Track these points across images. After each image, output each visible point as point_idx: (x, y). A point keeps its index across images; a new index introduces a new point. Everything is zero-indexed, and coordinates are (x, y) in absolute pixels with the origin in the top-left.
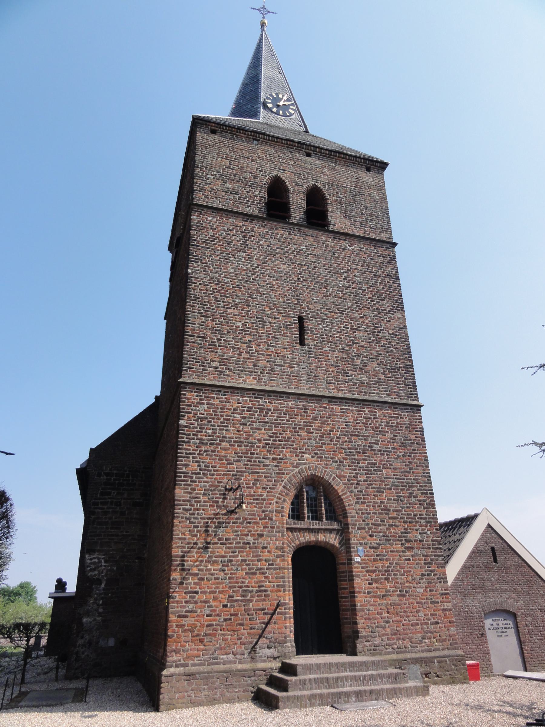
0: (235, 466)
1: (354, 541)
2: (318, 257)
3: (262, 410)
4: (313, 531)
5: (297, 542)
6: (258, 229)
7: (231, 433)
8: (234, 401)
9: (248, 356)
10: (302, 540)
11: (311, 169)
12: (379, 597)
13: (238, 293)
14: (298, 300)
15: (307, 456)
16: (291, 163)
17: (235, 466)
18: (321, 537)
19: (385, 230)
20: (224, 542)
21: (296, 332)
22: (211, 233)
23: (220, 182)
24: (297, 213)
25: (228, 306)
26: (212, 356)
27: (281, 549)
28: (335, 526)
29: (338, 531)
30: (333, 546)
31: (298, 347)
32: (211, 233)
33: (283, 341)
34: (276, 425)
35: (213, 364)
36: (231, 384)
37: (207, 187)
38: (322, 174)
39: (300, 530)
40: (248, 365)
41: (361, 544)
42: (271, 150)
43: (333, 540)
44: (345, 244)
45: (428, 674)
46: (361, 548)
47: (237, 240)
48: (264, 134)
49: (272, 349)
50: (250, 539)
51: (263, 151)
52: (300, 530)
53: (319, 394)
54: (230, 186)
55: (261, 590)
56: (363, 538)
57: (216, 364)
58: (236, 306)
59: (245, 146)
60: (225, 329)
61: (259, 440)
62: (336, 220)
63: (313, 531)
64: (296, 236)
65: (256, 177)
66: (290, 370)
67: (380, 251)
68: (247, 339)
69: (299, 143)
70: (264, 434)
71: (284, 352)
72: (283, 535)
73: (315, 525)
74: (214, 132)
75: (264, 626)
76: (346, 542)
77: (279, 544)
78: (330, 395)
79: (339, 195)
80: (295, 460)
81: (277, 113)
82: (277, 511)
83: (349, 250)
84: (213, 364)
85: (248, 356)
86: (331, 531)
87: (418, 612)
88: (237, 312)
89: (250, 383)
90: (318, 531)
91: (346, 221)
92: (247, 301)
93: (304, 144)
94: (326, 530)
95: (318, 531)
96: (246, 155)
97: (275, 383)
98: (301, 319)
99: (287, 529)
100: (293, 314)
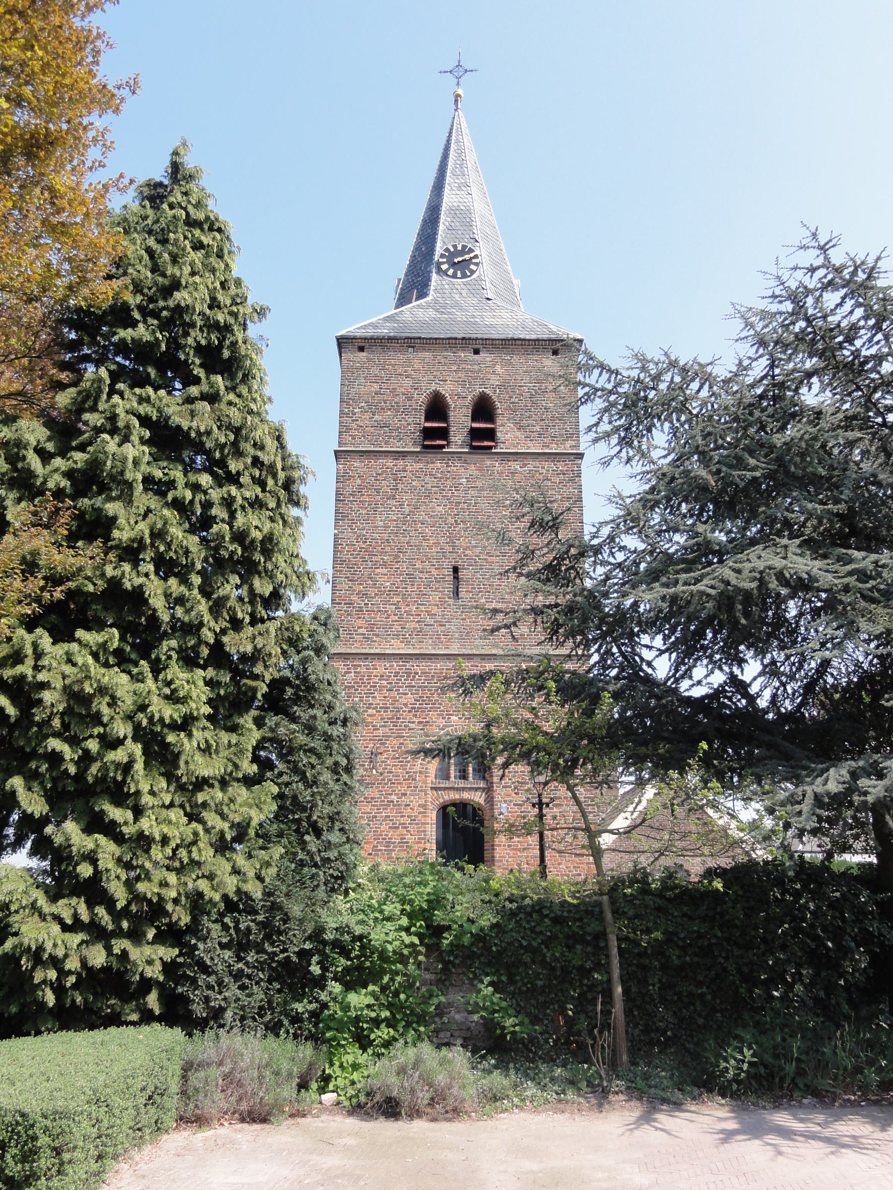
0: (381, 732)
1: (497, 798)
2: (482, 489)
3: (409, 674)
4: (458, 789)
5: (441, 800)
6: (412, 465)
7: (378, 699)
8: (381, 667)
9: (396, 618)
10: (446, 798)
11: (479, 371)
12: (519, 850)
13: (388, 549)
14: (454, 547)
15: (454, 718)
16: (454, 368)
17: (381, 732)
18: (466, 796)
19: (570, 437)
20: (370, 800)
21: (449, 587)
22: (359, 482)
23: (367, 416)
24: (458, 438)
25: (376, 565)
26: (360, 622)
27: (424, 806)
28: (482, 784)
29: (484, 789)
30: (479, 804)
31: (451, 601)
32: (359, 482)
33: (435, 597)
34: (423, 688)
35: (360, 631)
36: (377, 651)
37: (354, 426)
38: (494, 375)
39: (445, 789)
40: (397, 627)
41: (505, 802)
42: (427, 355)
43: (478, 798)
44: (516, 466)
45: (204, 751)
46: (504, 805)
47: (386, 485)
48: (420, 338)
49: (422, 608)
50: (394, 798)
51: (420, 359)
52: (445, 789)
53: (470, 652)
54: (380, 418)
55: (403, 842)
56: (508, 795)
57: (363, 631)
58: (385, 565)
59: (396, 358)
60: (372, 592)
61: (406, 705)
62: (508, 435)
63: (458, 789)
64: (456, 467)
65: (410, 399)
66: (440, 629)
67: (561, 467)
68: (395, 600)
69: (464, 339)
70: (410, 698)
71: (435, 610)
72: (426, 794)
73: (461, 784)
74: (361, 349)
75: (39, 663)
76: (490, 800)
77: (422, 802)
78: (483, 652)
79: (513, 400)
80: (441, 722)
81: (454, 276)
82: (421, 772)
83: (520, 473)
84: (360, 631)
85: (396, 618)
86: (476, 789)
87: (559, 864)
88: (385, 571)
89: (397, 647)
90: (464, 789)
91: (518, 434)
92: (397, 556)
93: (470, 339)
94: (471, 789)
95: (464, 789)
96: (400, 371)
97: (423, 645)
98: (456, 570)
99: (432, 788)
100: (448, 565)
